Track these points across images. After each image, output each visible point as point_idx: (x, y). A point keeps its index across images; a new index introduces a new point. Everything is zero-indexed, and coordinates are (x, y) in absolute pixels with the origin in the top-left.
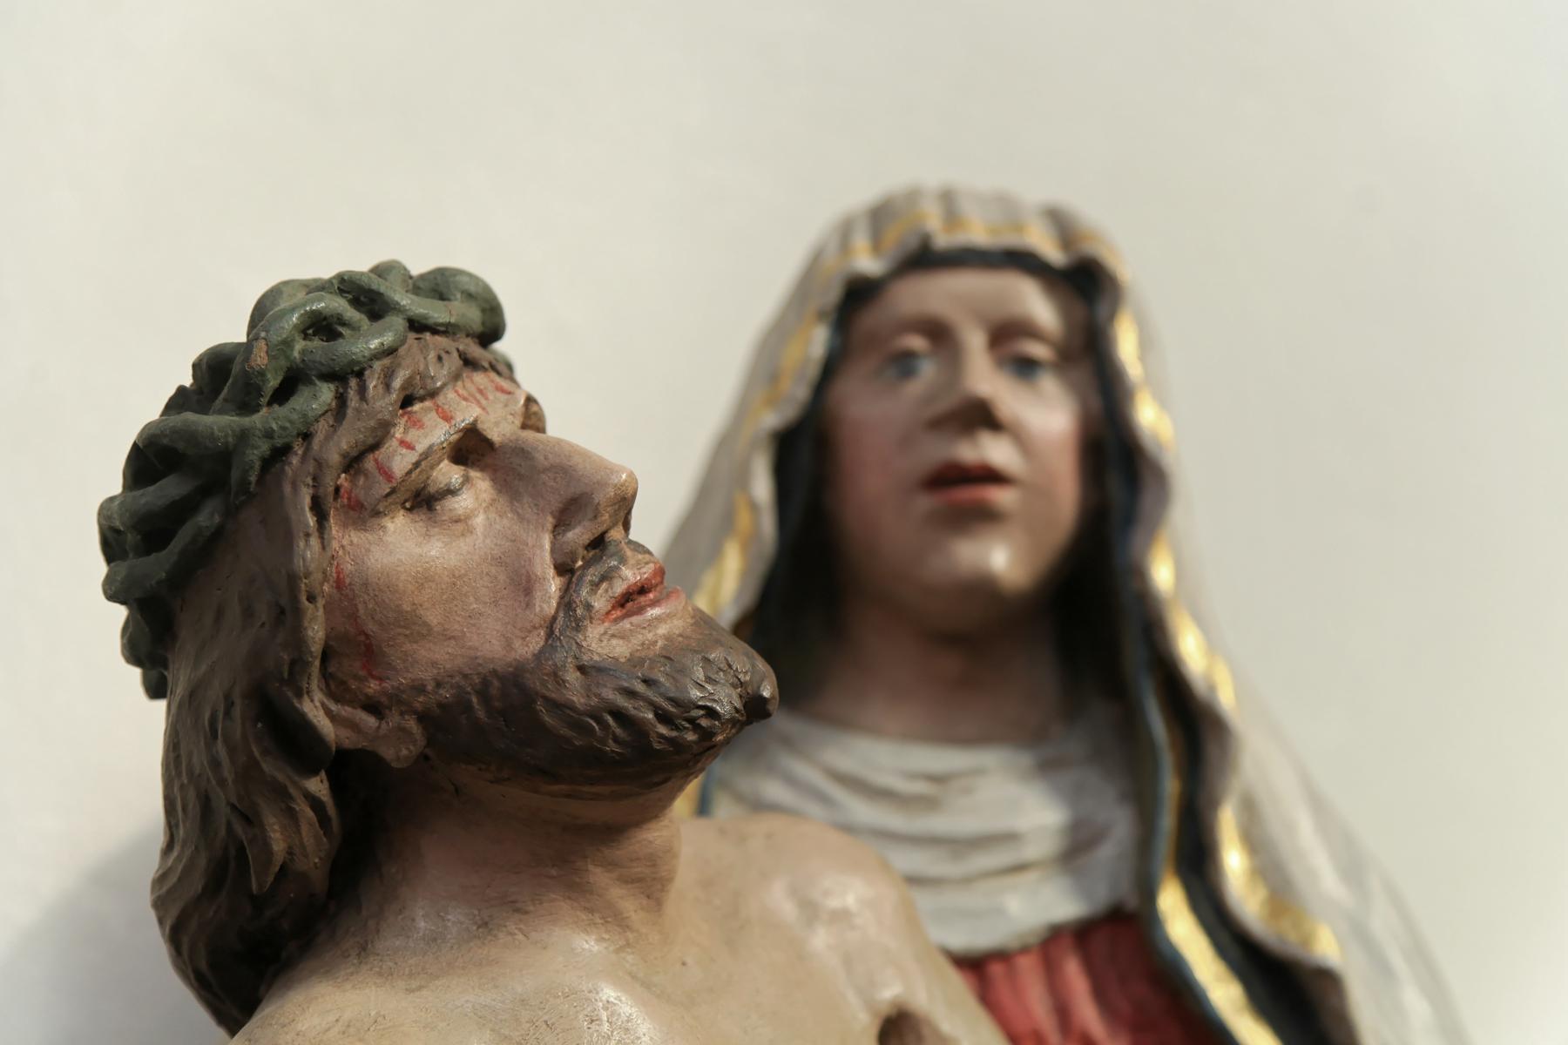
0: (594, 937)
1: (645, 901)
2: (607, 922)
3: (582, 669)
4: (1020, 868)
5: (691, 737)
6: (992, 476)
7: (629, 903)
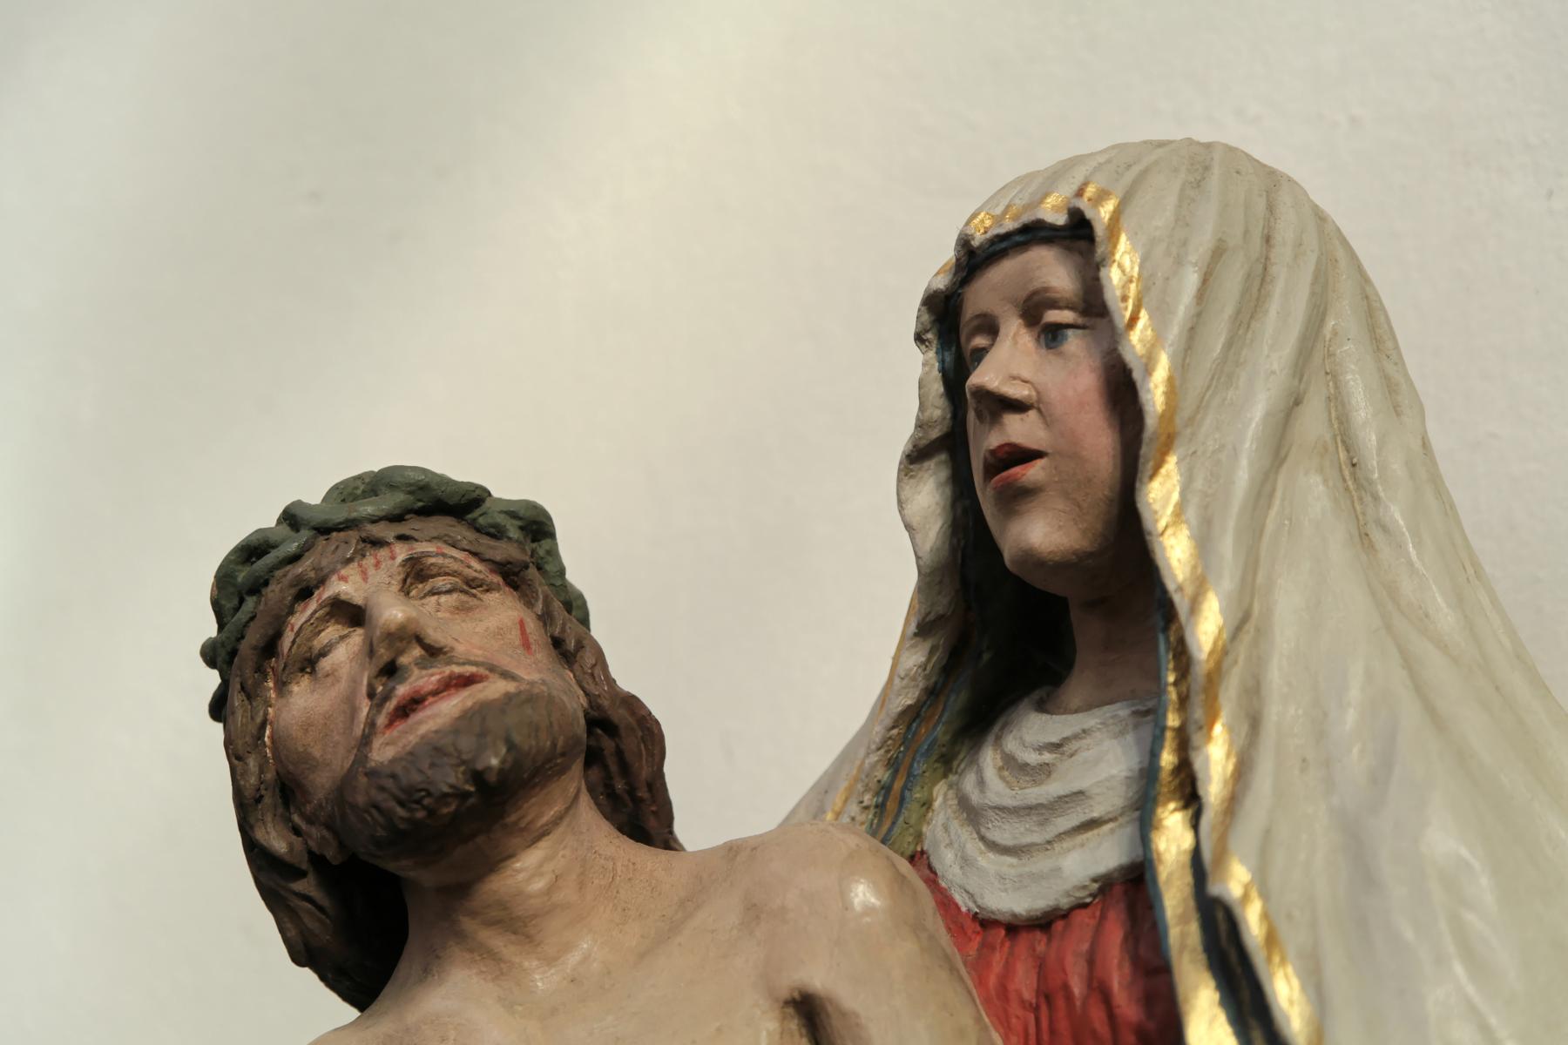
0: (475, 971)
1: (513, 937)
2: (484, 958)
3: (366, 774)
4: (1091, 824)
5: (420, 814)
6: (1026, 456)
7: (497, 941)
